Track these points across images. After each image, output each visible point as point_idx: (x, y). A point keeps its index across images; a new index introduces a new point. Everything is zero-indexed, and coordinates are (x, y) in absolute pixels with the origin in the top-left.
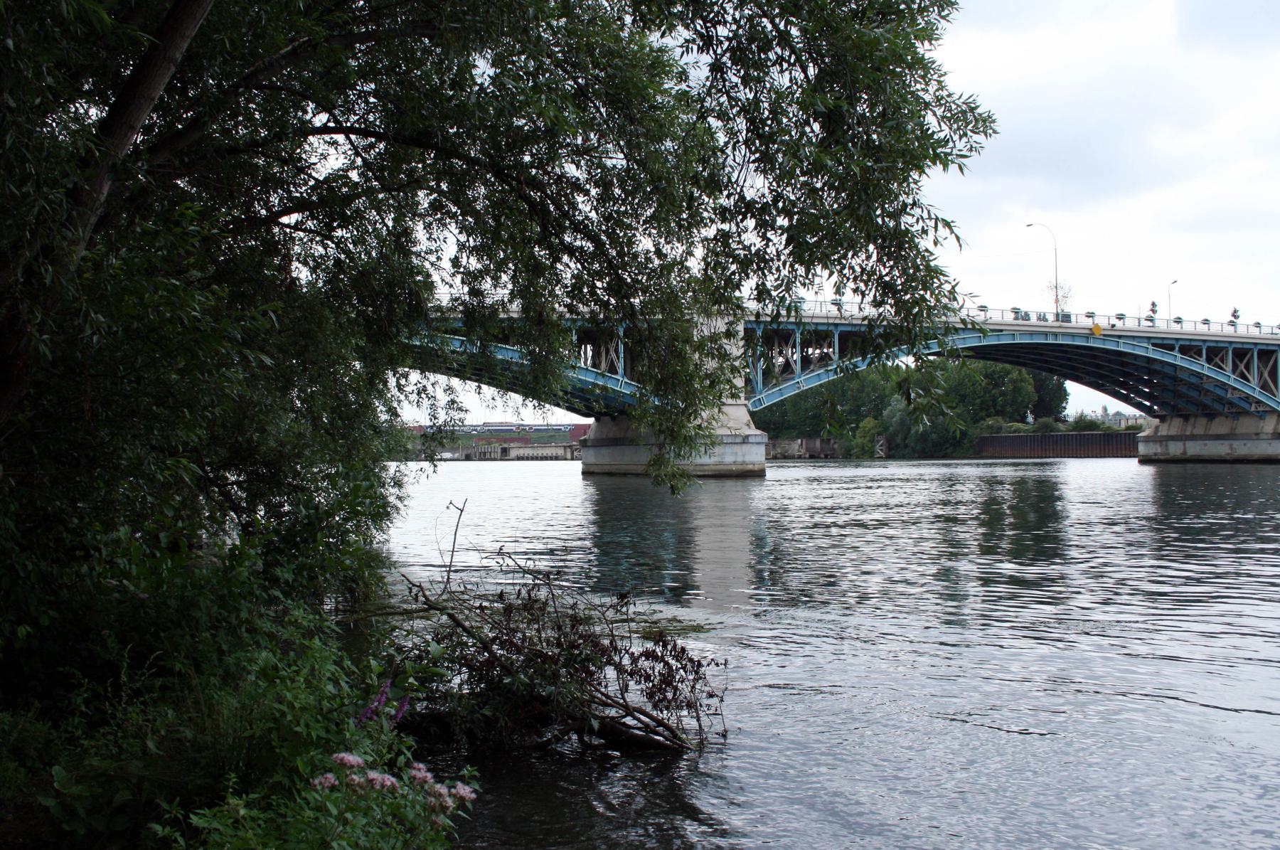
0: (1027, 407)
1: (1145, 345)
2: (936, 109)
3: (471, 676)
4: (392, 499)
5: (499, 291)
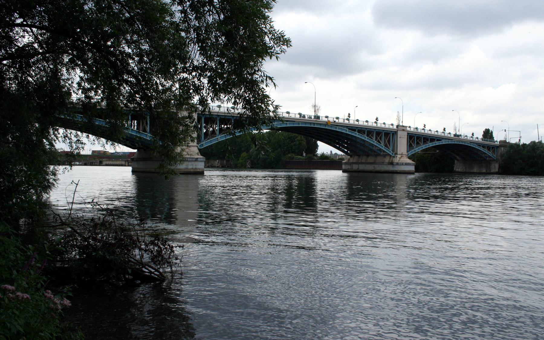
0: (303, 150)
1: (346, 129)
2: (269, 35)
3: (80, 251)
4: (51, 181)
5: (97, 97)
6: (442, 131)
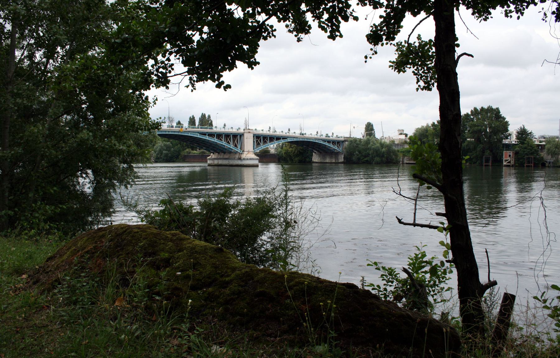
6: (287, 131)
